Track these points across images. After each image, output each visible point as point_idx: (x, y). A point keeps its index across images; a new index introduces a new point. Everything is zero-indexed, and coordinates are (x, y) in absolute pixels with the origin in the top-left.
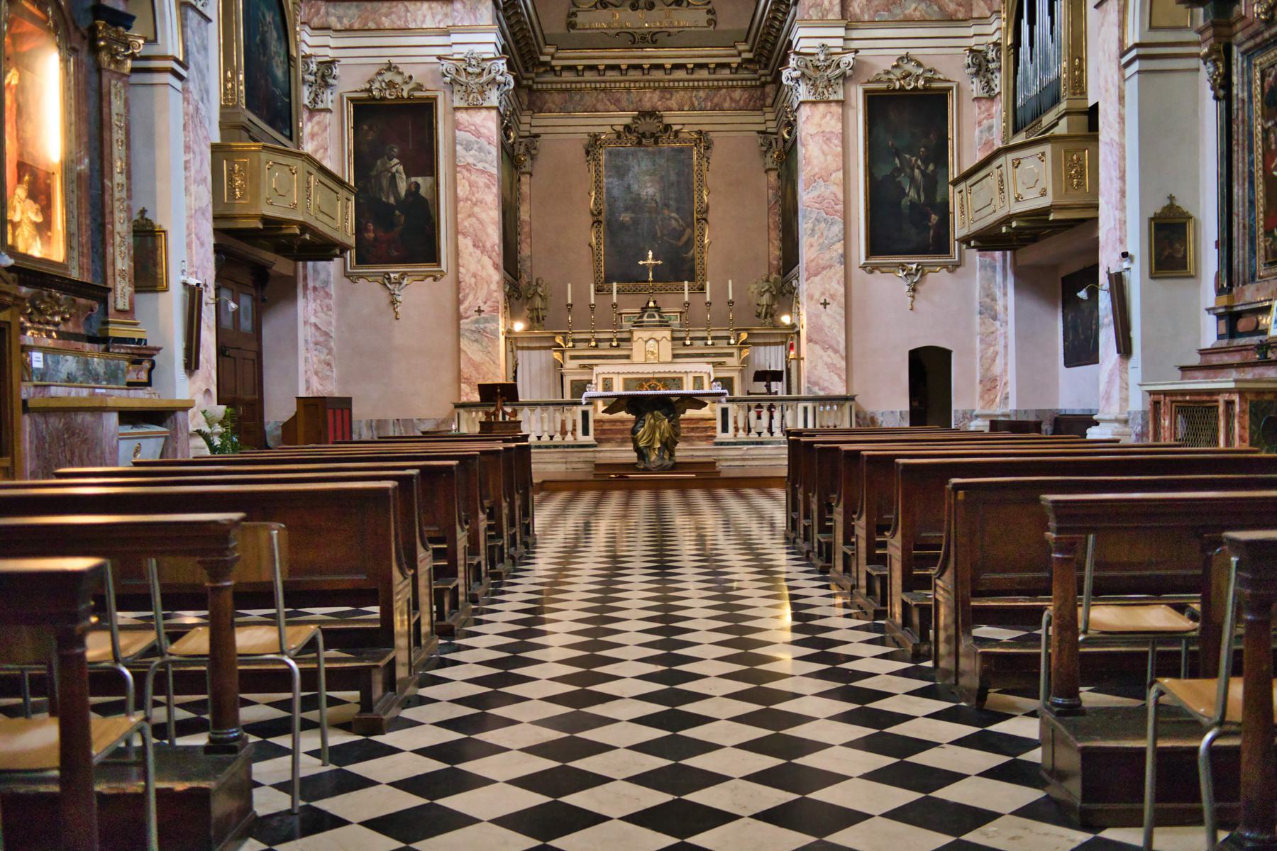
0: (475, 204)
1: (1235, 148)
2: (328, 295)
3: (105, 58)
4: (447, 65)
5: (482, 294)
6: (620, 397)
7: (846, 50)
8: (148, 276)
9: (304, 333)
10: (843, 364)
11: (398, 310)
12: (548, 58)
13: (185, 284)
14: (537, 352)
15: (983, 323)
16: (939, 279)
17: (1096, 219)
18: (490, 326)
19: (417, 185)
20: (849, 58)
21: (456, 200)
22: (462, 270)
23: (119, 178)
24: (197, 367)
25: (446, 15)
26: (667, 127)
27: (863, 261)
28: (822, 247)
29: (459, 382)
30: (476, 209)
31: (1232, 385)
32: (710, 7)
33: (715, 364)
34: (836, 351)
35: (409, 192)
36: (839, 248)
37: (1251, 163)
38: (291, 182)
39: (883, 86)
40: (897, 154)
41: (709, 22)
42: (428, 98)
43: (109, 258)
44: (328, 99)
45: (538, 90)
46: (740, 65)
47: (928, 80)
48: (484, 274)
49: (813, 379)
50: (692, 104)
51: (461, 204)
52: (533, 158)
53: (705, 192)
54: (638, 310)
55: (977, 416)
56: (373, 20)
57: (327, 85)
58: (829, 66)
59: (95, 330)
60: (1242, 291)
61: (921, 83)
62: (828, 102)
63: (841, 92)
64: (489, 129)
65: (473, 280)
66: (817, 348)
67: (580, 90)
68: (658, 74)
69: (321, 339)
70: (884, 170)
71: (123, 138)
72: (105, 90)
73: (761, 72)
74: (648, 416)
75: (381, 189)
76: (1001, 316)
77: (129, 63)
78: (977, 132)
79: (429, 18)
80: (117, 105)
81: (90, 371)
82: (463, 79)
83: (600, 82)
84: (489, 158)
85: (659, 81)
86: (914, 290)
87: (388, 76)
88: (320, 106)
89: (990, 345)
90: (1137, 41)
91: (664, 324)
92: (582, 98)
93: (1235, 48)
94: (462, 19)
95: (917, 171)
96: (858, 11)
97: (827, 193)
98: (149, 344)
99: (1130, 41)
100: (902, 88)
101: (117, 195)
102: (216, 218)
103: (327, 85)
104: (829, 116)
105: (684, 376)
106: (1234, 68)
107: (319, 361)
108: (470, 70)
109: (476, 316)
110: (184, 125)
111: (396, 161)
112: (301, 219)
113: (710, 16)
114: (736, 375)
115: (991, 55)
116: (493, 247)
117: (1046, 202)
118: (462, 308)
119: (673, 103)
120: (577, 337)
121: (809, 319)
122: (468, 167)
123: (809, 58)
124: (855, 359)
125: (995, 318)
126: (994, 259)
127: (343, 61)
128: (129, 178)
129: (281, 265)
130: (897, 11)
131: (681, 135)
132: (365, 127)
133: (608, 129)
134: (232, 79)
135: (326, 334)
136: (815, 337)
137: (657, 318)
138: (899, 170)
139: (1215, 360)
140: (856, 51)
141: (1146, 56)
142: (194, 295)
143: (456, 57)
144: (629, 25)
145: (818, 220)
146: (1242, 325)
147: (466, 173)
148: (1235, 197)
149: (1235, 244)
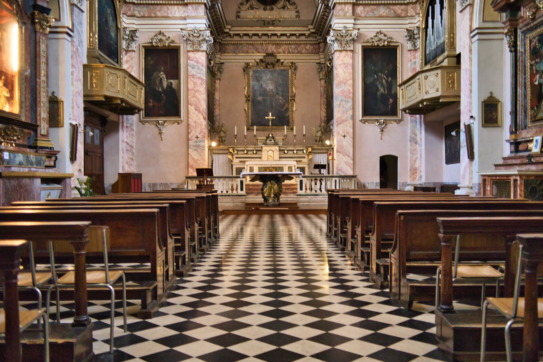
0: (196, 92)
1: (518, 72)
2: (132, 130)
3: (38, 27)
4: (185, 32)
5: (198, 130)
6: (256, 175)
8: (55, 120)
10: (352, 162)
11: (162, 136)
12: (228, 30)
13: (71, 124)
14: (222, 155)
15: (411, 145)
16: (393, 126)
18: (202, 144)
19: (171, 83)
21: (188, 90)
22: (190, 120)
23: (43, 78)
24: (75, 159)
25: (185, 11)
26: (278, 61)
27: (361, 118)
28: (343, 112)
30: (196, 94)
31: (517, 173)
34: (349, 156)
35: (168, 86)
36: (351, 112)
37: (525, 79)
38: (117, 81)
39: (370, 44)
41: (297, 16)
42: (176, 46)
43: (38, 113)
45: (224, 44)
46: (309, 35)
47: (389, 42)
48: (199, 122)
49: (339, 168)
51: (190, 92)
52: (221, 72)
53: (294, 88)
55: (408, 185)
57: (133, 40)
58: (347, 35)
59: (32, 143)
60: (521, 133)
61: (386, 43)
62: (347, 51)
64: (202, 60)
65: (195, 124)
66: (341, 155)
67: (241, 44)
68: (275, 38)
69: (129, 148)
70: (370, 80)
71: (45, 61)
73: (318, 38)
76: (419, 142)
77: (48, 29)
78: (409, 64)
79: (177, 12)
80: (43, 47)
81: (29, 161)
82: (191, 38)
84: (202, 72)
85: (275, 41)
87: (160, 37)
88: (130, 49)
89: (414, 154)
91: (276, 144)
92: (242, 48)
93: (518, 30)
94: (192, 13)
96: (359, 12)
98: (55, 149)
101: (42, 85)
103: (133, 40)
104: (347, 57)
106: (518, 39)
108: (194, 35)
109: (196, 139)
110: (72, 57)
111: (162, 73)
112: (121, 97)
113: (297, 14)
116: (203, 110)
118: (190, 136)
119: (281, 50)
120: (239, 149)
122: (193, 76)
123: (338, 32)
125: (416, 143)
126: (416, 118)
127: (140, 30)
128: (47, 78)
129: (112, 117)
130: (376, 13)
131: (284, 64)
132: (150, 58)
133: (253, 61)
135: (132, 146)
136: (340, 150)
137: (273, 141)
139: (509, 162)
140: (359, 29)
141: (481, 33)
142: (74, 128)
144: (262, 17)
145: (342, 101)
147: (192, 78)
149: (518, 113)
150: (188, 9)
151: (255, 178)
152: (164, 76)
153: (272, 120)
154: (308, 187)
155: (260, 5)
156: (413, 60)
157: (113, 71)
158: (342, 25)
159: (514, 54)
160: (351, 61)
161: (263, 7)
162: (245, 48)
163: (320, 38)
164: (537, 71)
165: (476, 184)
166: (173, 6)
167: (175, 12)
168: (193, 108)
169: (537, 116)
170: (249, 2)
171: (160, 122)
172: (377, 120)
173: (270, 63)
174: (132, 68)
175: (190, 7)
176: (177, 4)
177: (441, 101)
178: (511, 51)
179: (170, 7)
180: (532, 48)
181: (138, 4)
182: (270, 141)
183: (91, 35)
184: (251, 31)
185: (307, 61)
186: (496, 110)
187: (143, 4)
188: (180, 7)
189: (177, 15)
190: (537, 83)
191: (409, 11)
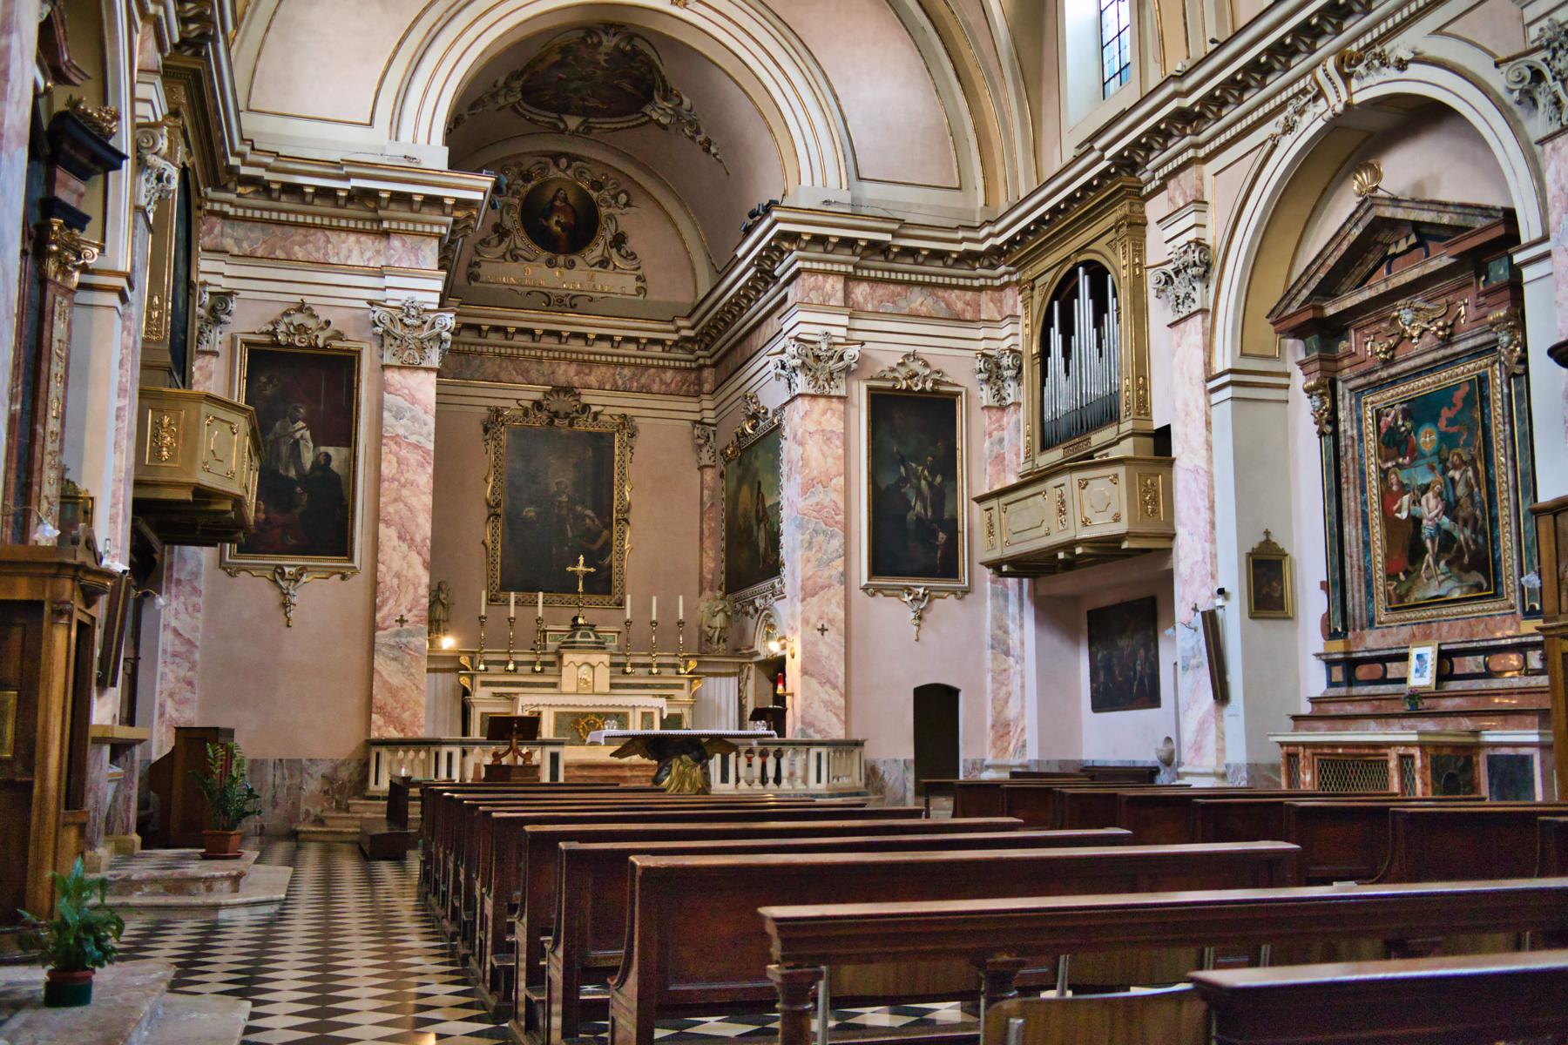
0: (404, 486)
1: (1345, 486)
2: (196, 592)
3: (52, 266)
5: (407, 599)
6: (635, 737)
7: (849, 342)
11: (291, 615)
15: (995, 659)
16: (946, 606)
17: (1169, 551)
19: (328, 457)
20: (854, 351)
21: (378, 479)
22: (381, 567)
23: (53, 425)
25: (378, 252)
26: (586, 407)
27: (865, 581)
29: (369, 713)
30: (405, 492)
31: (1415, 738)
32: (639, 272)
34: (835, 687)
35: (316, 465)
36: (839, 565)
37: (1364, 503)
38: (231, 444)
39: (890, 385)
40: (903, 461)
41: (639, 290)
42: (348, 350)
44: (217, 338)
46: (676, 343)
47: (936, 382)
48: (411, 575)
49: (808, 719)
50: (615, 382)
51: (385, 485)
55: (988, 767)
56: (283, 248)
58: (831, 357)
60: (1362, 638)
61: (929, 385)
62: (829, 397)
63: (843, 386)
65: (395, 581)
66: (814, 683)
67: (481, 354)
68: (578, 345)
69: (182, 649)
70: (888, 480)
72: (48, 308)
73: (699, 353)
74: (675, 763)
75: (278, 458)
76: (1015, 650)
77: (77, 277)
78: (987, 444)
79: (356, 252)
80: (60, 328)
82: (398, 330)
83: (506, 347)
85: (577, 352)
86: (920, 618)
87: (298, 319)
89: (1002, 684)
90: (1229, 366)
91: (600, 647)
92: (482, 364)
93: (1340, 384)
94: (400, 259)
96: (861, 299)
97: (826, 502)
99: (1218, 367)
100: (909, 389)
102: (138, 484)
103: (219, 322)
104: (829, 414)
106: (1340, 404)
107: (177, 679)
108: (407, 321)
109: (397, 627)
111: (301, 424)
114: (686, 712)
115: (1006, 361)
116: (424, 540)
117: (1121, 528)
118: (379, 616)
119: (592, 380)
121: (804, 647)
122: (396, 439)
124: (854, 697)
125: (1007, 653)
126: (1006, 586)
127: (243, 294)
128: (63, 425)
130: (902, 303)
131: (600, 418)
132: (263, 379)
133: (513, 404)
134: (160, 306)
135: (190, 643)
136: (810, 668)
137: (593, 639)
138: (905, 480)
139: (1333, 709)
140: (863, 344)
141: (1245, 383)
142: (1211, 622)
143: (389, 303)
146: (1362, 672)
147: (394, 447)
148: (1346, 537)
149: (1348, 586)
150: (391, 248)
151: (633, 744)
152: (307, 434)
153: (587, 576)
155: (538, 250)
156: (996, 434)
157: (221, 413)
158: (819, 329)
159: (1330, 441)
160: (840, 427)
161: (546, 255)
162: (490, 367)
163: (705, 353)
164: (1400, 483)
165: (1238, 768)
166: (343, 235)
167: (350, 251)
169: (1407, 595)
171: (287, 570)
172: (908, 588)
173: (562, 413)
175: (396, 242)
176: (356, 231)
177: (1125, 545)
178: (1321, 434)
179: (333, 236)
180: (1384, 430)
181: (235, 218)
183: (156, 300)
185: (664, 414)
186: (1279, 576)
187: (252, 220)
188: (363, 238)
189: (355, 260)
190: (1404, 515)
191: (983, 306)
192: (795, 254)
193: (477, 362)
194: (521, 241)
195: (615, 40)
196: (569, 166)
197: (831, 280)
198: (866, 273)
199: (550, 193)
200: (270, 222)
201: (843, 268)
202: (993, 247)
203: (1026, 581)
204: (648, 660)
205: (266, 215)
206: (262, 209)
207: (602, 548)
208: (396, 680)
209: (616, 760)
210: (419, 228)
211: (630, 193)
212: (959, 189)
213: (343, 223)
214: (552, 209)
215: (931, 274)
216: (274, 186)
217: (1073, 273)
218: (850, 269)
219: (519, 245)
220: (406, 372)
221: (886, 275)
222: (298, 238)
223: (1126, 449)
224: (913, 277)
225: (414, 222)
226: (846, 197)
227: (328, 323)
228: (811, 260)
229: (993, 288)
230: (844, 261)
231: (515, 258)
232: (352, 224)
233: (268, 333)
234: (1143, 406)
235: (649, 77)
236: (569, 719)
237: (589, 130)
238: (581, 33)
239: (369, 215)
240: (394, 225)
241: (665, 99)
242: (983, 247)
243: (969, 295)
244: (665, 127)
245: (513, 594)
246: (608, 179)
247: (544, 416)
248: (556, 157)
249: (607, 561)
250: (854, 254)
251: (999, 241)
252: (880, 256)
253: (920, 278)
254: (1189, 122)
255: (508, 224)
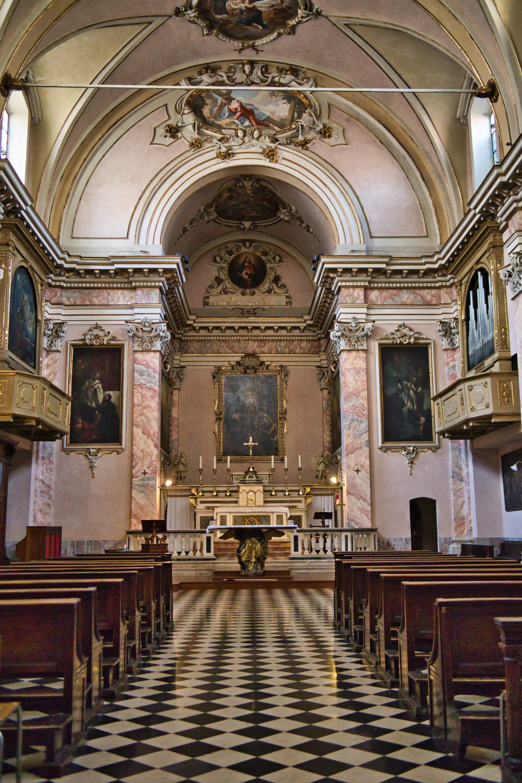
0: (145, 408)
2: (51, 462)
4: (131, 326)
5: (147, 463)
6: (230, 529)
7: (367, 321)
9: (34, 485)
12: (192, 322)
14: (180, 498)
18: (151, 483)
19: (110, 396)
20: (369, 325)
22: (135, 447)
25: (132, 297)
26: (262, 363)
27: (380, 444)
29: (130, 518)
33: (290, 507)
34: (365, 500)
35: (104, 400)
36: (366, 437)
38: (32, 396)
39: (390, 342)
40: (400, 381)
41: (287, 303)
42: (118, 345)
46: (305, 328)
47: (416, 339)
48: (148, 450)
49: (351, 517)
52: (181, 380)
53: (284, 402)
54: (243, 473)
55: (453, 542)
56: (88, 300)
58: (358, 330)
62: (358, 350)
64: (154, 363)
65: (141, 454)
66: (353, 498)
67: (210, 340)
69: (45, 489)
70: (392, 391)
73: (317, 332)
74: (248, 542)
75: (87, 398)
76: (465, 479)
78: (446, 369)
82: (140, 334)
87: (95, 332)
88: (54, 348)
91: (259, 482)
92: (211, 345)
94: (141, 300)
95: (411, 391)
96: (374, 299)
100: (401, 343)
103: (59, 337)
104: (358, 359)
105: (271, 514)
107: (43, 503)
108: (144, 329)
109: (142, 476)
111: (97, 381)
112: (37, 416)
113: (288, 300)
114: (303, 514)
115: (453, 325)
116: (154, 434)
117: (489, 411)
118: (134, 471)
119: (265, 349)
120: (205, 489)
121: (348, 480)
122: (141, 386)
123: (346, 325)
125: (462, 480)
126: (460, 444)
129: (23, 443)
130: (397, 299)
131: (270, 368)
133: (227, 364)
135: (49, 486)
136: (352, 491)
137: (255, 478)
138: (401, 391)
140: (374, 321)
143: (136, 321)
144: (240, 304)
147: (140, 390)
150: (136, 295)
151: (229, 533)
152: (100, 386)
154: (306, 546)
155: (237, 287)
156: (451, 364)
157: (27, 380)
158: (351, 316)
161: (240, 290)
166: (116, 291)
167: (119, 298)
168: (140, 431)
170: (222, 285)
171: (91, 450)
172: (404, 447)
173: (250, 367)
174: (55, 374)
175: (139, 292)
176: (121, 288)
177: (493, 421)
179: (111, 292)
181: (67, 288)
182: (250, 477)
184: (224, 322)
185: (307, 364)
187: (74, 288)
192: (337, 279)
193: (209, 345)
194: (228, 284)
195: (251, 183)
196: (250, 246)
197: (357, 291)
198: (376, 285)
199: (242, 260)
200: (82, 288)
201: (363, 284)
202: (441, 265)
203: (468, 441)
204: (284, 488)
205: (80, 285)
206: (78, 283)
207: (274, 431)
208: (142, 502)
209: (222, 540)
210: (149, 284)
211: (281, 256)
212: (427, 236)
213: (115, 285)
214: (243, 267)
215: (412, 283)
216: (81, 272)
217: (475, 277)
218: (367, 284)
219: (228, 286)
220: (144, 353)
221: (387, 285)
222: (95, 294)
223: (496, 368)
224: (402, 285)
225: (147, 282)
226: (363, 247)
227: (109, 333)
228: (345, 281)
229: (446, 287)
230: (363, 280)
231: (226, 293)
232: (119, 286)
233: (82, 340)
234: (505, 344)
235: (274, 198)
236: (240, 519)
237: (256, 227)
238: (234, 182)
239: (126, 280)
240: (138, 284)
241: (284, 208)
242: (436, 266)
243: (434, 291)
244: (288, 222)
245: (229, 457)
246: (270, 250)
247: (241, 369)
248: (244, 242)
249: (275, 439)
250: (368, 276)
251: (443, 262)
252: (381, 275)
253: (406, 285)
254: (511, 189)
255: (222, 277)
